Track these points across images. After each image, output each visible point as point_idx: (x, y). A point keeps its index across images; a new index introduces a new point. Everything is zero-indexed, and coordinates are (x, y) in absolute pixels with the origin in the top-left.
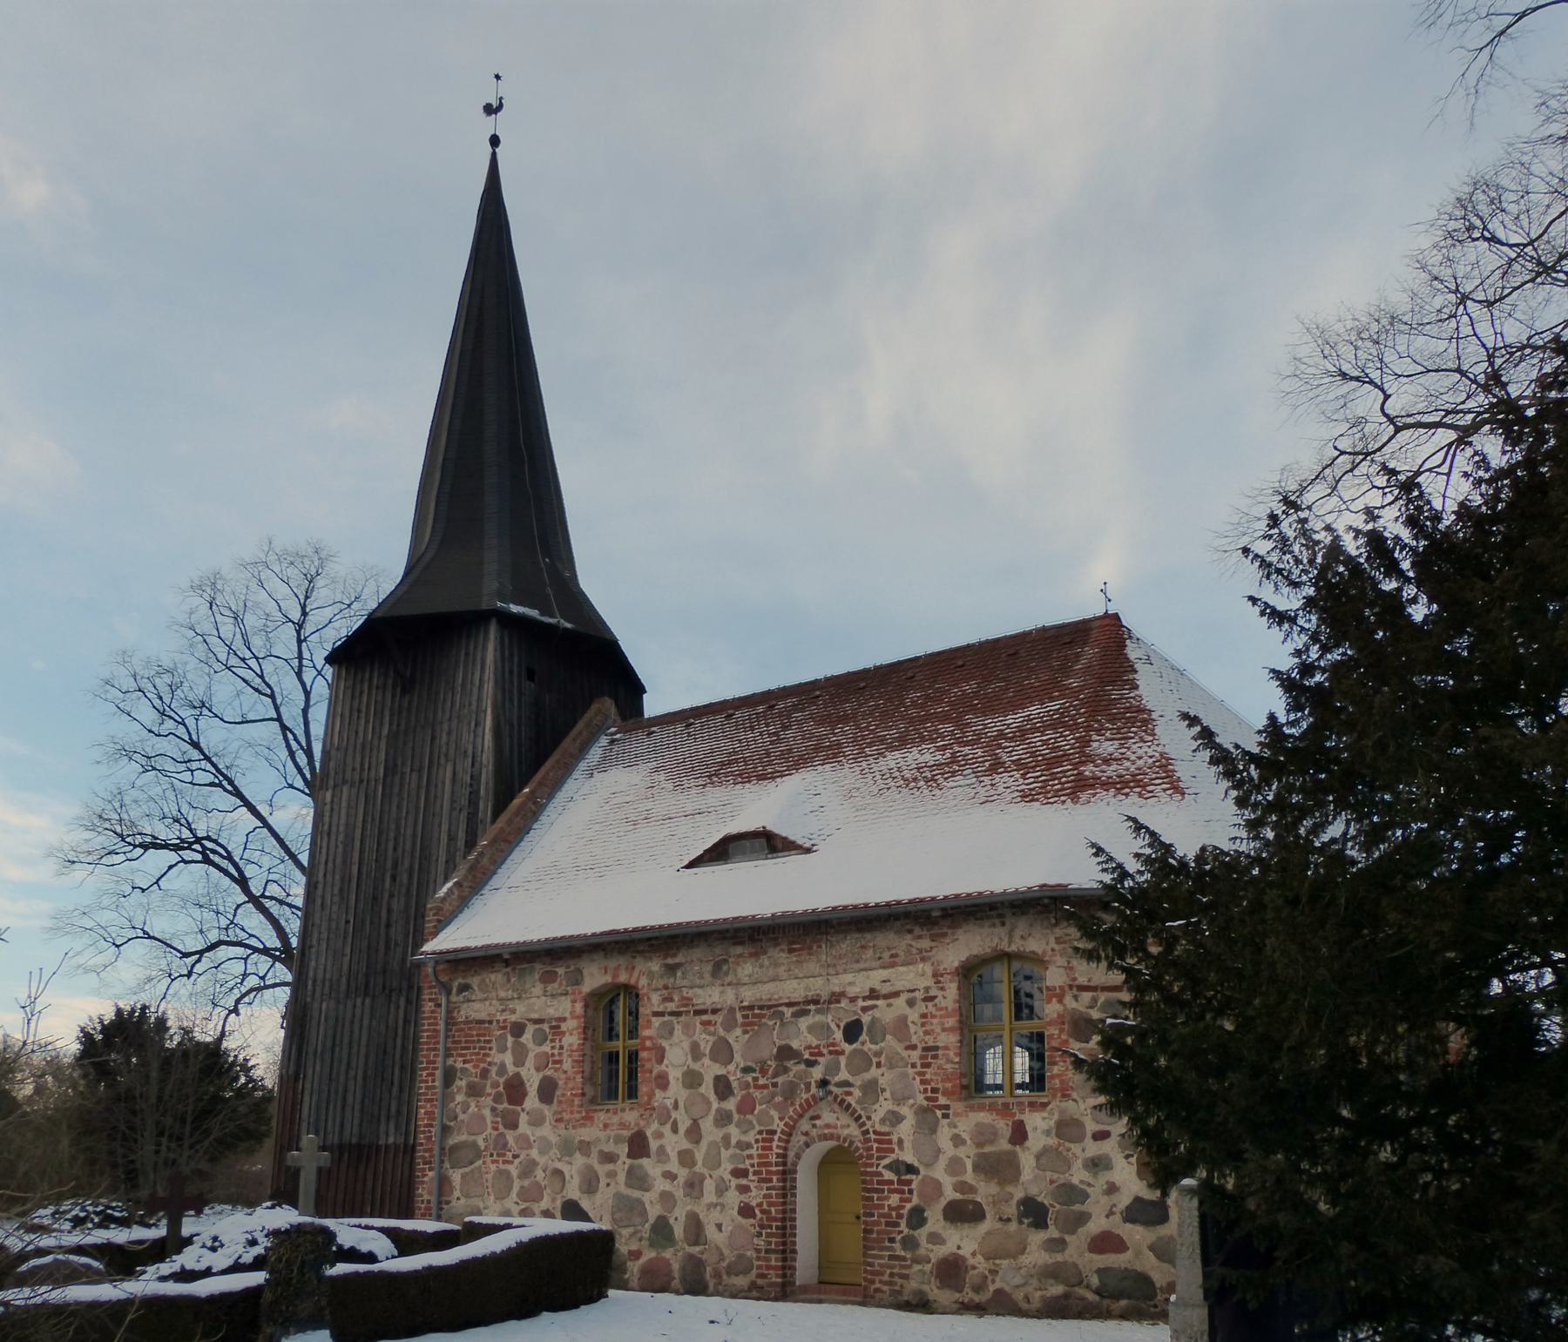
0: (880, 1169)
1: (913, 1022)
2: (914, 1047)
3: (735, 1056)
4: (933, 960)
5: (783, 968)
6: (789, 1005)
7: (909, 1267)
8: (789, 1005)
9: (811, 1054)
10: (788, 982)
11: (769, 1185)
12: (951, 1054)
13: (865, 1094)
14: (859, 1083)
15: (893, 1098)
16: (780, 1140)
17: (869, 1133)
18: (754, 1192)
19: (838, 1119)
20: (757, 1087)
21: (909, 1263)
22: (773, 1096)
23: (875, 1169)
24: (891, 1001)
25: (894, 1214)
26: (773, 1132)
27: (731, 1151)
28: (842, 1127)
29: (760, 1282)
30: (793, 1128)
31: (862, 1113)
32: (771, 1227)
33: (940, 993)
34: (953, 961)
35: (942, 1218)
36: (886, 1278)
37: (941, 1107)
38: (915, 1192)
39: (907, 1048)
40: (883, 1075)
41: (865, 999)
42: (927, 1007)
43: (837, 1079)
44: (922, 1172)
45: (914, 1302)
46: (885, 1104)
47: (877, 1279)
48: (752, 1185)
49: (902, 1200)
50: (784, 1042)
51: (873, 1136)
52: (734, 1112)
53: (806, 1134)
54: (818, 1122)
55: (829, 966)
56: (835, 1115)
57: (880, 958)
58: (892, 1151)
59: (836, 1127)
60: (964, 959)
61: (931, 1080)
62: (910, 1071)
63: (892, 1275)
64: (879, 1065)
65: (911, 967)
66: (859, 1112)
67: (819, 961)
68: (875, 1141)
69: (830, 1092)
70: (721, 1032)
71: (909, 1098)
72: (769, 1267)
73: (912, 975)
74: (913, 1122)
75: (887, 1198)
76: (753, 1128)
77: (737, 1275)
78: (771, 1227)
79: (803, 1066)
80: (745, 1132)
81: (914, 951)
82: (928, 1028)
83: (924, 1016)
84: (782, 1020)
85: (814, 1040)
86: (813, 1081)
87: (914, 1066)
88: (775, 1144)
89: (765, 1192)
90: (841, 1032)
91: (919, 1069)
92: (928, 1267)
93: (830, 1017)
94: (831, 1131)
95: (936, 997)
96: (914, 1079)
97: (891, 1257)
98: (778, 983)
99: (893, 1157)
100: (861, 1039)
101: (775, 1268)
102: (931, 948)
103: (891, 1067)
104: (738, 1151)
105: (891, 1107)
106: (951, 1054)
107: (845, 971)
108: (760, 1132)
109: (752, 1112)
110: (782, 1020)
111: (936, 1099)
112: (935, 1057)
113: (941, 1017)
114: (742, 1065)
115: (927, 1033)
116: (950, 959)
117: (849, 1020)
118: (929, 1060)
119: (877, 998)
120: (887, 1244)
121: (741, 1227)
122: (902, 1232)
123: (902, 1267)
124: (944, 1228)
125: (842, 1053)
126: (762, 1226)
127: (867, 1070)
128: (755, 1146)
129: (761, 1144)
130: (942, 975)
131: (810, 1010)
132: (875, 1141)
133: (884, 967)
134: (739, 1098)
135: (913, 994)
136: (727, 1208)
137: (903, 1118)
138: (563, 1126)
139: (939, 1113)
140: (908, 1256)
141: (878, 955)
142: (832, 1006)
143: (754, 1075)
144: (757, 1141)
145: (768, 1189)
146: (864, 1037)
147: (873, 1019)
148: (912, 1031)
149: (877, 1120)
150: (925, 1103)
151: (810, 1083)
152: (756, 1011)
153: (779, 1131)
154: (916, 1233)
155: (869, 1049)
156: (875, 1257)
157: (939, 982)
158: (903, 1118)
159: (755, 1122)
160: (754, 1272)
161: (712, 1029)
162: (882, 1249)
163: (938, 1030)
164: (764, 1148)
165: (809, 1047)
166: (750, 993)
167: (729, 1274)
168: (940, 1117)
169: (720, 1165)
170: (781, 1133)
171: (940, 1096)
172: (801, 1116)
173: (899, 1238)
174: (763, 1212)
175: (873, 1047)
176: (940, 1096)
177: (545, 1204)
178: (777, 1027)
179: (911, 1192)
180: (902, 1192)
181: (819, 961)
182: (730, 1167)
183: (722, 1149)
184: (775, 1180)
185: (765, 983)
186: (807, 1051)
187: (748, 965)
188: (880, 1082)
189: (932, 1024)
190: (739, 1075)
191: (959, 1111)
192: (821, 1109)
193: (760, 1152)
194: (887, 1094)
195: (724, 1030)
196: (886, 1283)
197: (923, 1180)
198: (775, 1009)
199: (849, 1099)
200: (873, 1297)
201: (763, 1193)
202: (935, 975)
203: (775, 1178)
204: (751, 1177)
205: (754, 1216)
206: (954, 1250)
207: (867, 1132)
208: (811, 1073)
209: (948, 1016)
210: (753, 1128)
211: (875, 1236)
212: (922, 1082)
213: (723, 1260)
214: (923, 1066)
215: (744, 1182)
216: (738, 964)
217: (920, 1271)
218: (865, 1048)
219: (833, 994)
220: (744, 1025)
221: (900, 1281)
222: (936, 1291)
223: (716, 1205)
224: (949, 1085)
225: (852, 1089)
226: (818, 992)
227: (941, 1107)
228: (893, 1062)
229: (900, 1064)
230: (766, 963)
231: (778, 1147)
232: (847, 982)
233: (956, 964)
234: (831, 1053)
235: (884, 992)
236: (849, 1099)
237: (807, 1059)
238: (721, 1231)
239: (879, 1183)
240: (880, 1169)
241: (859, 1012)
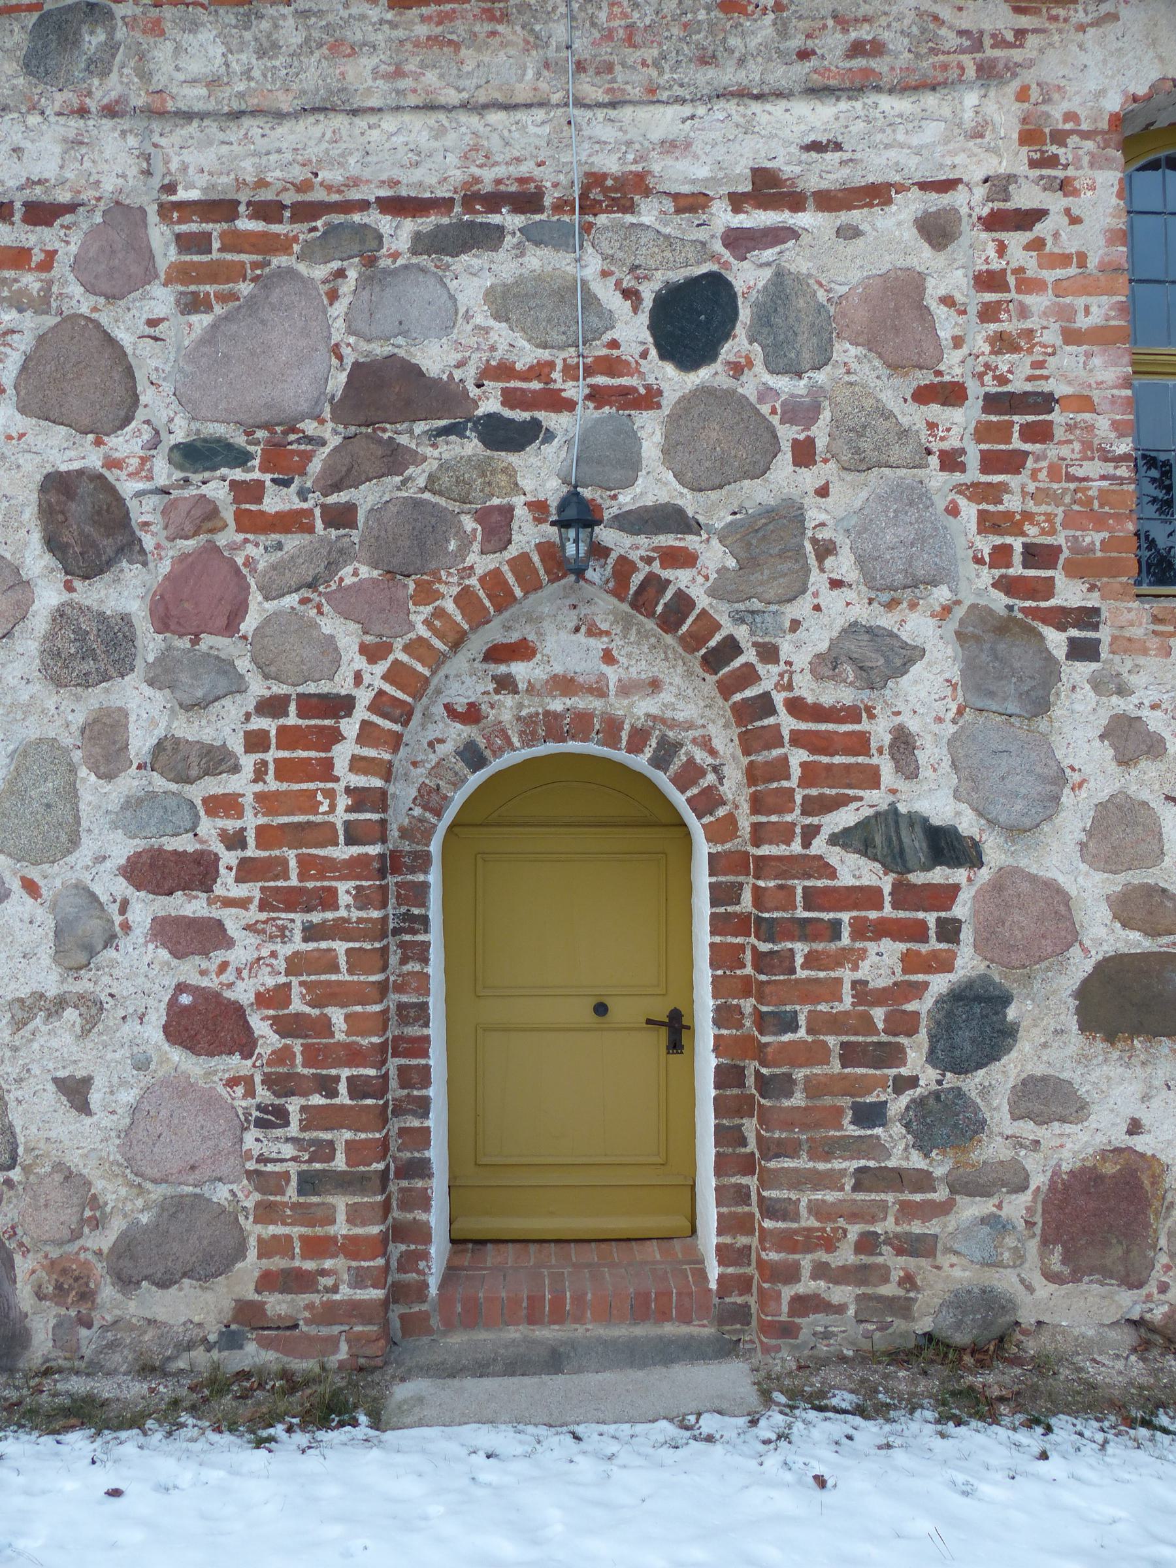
0: (819, 846)
1: (948, 301)
2: (953, 394)
3: (147, 396)
4: (1028, 77)
5: (367, 63)
6: (397, 206)
7: (945, 1208)
8: (397, 206)
9: (510, 398)
10: (389, 123)
11: (316, 917)
12: (1103, 424)
13: (748, 564)
14: (722, 519)
15: (869, 580)
16: (367, 734)
17: (772, 711)
18: (243, 950)
19: (608, 658)
20: (252, 523)
21: (941, 1194)
22: (336, 559)
23: (796, 847)
24: (855, 216)
25: (878, 1014)
26: (342, 705)
27: (130, 783)
28: (625, 689)
29: (278, 1304)
30: (417, 686)
31: (742, 633)
32: (328, 1086)
33: (1055, 203)
34: (1101, 93)
35: (1072, 1023)
36: (845, 1256)
37: (1061, 618)
38: (967, 934)
39: (923, 395)
40: (823, 492)
41: (737, 202)
42: (1002, 249)
43: (627, 500)
44: (995, 852)
45: (961, 1338)
46: (833, 600)
47: (806, 1262)
48: (232, 921)
49: (910, 962)
50: (380, 350)
51: (787, 723)
52: (143, 626)
53: (471, 715)
54: (519, 670)
55: (580, 67)
56: (598, 644)
57: (804, 55)
58: (872, 779)
59: (601, 693)
60: (1142, 90)
61: (1028, 516)
62: (937, 480)
63: (867, 1244)
64: (804, 454)
65: (930, 100)
66: (728, 627)
67: (537, 41)
68: (798, 739)
69: (599, 551)
70: (79, 300)
71: (934, 583)
72: (317, 1247)
73: (932, 131)
74: (954, 672)
75: (853, 958)
76: (238, 687)
77: (164, 1284)
78: (328, 1086)
79: (471, 446)
80: (196, 706)
81: (951, 40)
82: (1009, 325)
83: (988, 281)
84: (371, 262)
85: (522, 343)
86: (518, 501)
87: (951, 461)
88: (342, 754)
89: (298, 944)
90: (644, 318)
91: (973, 474)
92: (1016, 1206)
93: (593, 264)
94: (581, 703)
95: (1039, 215)
96: (953, 511)
97: (863, 1180)
98: (339, 121)
99: (875, 799)
100: (728, 351)
101: (352, 1248)
102: (1020, 33)
103: (860, 465)
104: (160, 783)
105: (861, 613)
106: (1103, 424)
107: (652, 96)
108: (272, 706)
109: (230, 627)
110: (371, 262)
111: (1046, 588)
112: (1040, 433)
113: (1060, 288)
114: (179, 437)
115: (1003, 343)
116: (1092, 85)
117: (679, 276)
118: (1016, 443)
119: (796, 202)
120: (853, 1130)
121: (181, 1088)
122: (913, 1082)
123: (907, 1211)
124: (1083, 1059)
125: (649, 399)
126: (282, 1084)
127: (760, 471)
128: (248, 762)
129: (272, 755)
130: (1060, 138)
131: (500, 229)
132: (798, 739)
133: (816, 92)
134: (165, 567)
135: (945, 200)
136: (112, 1016)
137: (911, 655)
138: (995, 1114)
139: (1056, 640)
140: (939, 1171)
141: (796, 43)
142: (602, 219)
143: (238, 474)
144: (256, 742)
145: (311, 933)
146: (738, 345)
147: (780, 275)
148: (945, 333)
149: (801, 660)
150: (999, 601)
151: (507, 512)
152: (245, 224)
153: (364, 698)
154: (971, 1084)
155: (766, 393)
156: (799, 1180)
157: (1052, 161)
158: (911, 655)
159: (243, 665)
160: (251, 1265)
161: (31, 281)
162: (825, 1150)
163: (1052, 336)
164: (285, 770)
165: (504, 371)
166: (207, 158)
167: (126, 1282)
168: (1060, 652)
169: (74, 842)
170: (373, 708)
171: (1058, 575)
172: (458, 642)
173: (898, 1105)
174: (287, 1026)
175: (783, 384)
176: (1058, 575)
177: (973, 575)
178: (347, 287)
179: (950, 931)
180: (917, 932)
181: (537, 41)
182: (122, 848)
183: (83, 772)
184: (344, 899)
185: (280, 116)
186: (494, 388)
187: (206, 35)
188: (814, 516)
189: (1024, 312)
190: (163, 472)
191: (1138, 632)
192: (533, 619)
193: (272, 784)
194: (844, 565)
195: (90, 289)
196: (842, 1276)
197: (998, 886)
198: (337, 219)
199: (681, 578)
200: (788, 1331)
201: (285, 950)
202: (1029, 137)
203: (344, 890)
204: (227, 885)
205: (246, 1044)
206: (1121, 1139)
207: (764, 705)
208: (510, 472)
209: (1087, 287)
210: (238, 687)
211: (798, 1100)
212: (988, 524)
213: (97, 1224)
214: (989, 463)
215: (194, 906)
216: (156, 29)
217: (984, 1220)
218: (748, 388)
219: (595, 179)
220: (180, 274)
221: (898, 1265)
222: (1044, 1289)
223: (61, 1003)
224: (1094, 538)
225: (691, 542)
226: (524, 169)
227: (1061, 618)
228: (866, 445)
229: (897, 453)
230: (291, 35)
231: (357, 764)
232: (656, 136)
233: (1114, 103)
234: (597, 396)
235: (813, 183)
236: (681, 578)
237: (492, 418)
238: (84, 1108)
239: (812, 899)
240: (819, 846)
241: (718, 247)
